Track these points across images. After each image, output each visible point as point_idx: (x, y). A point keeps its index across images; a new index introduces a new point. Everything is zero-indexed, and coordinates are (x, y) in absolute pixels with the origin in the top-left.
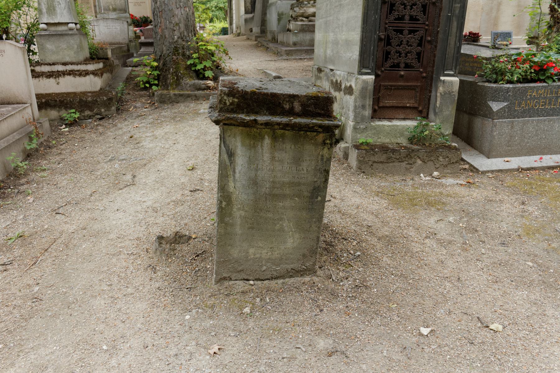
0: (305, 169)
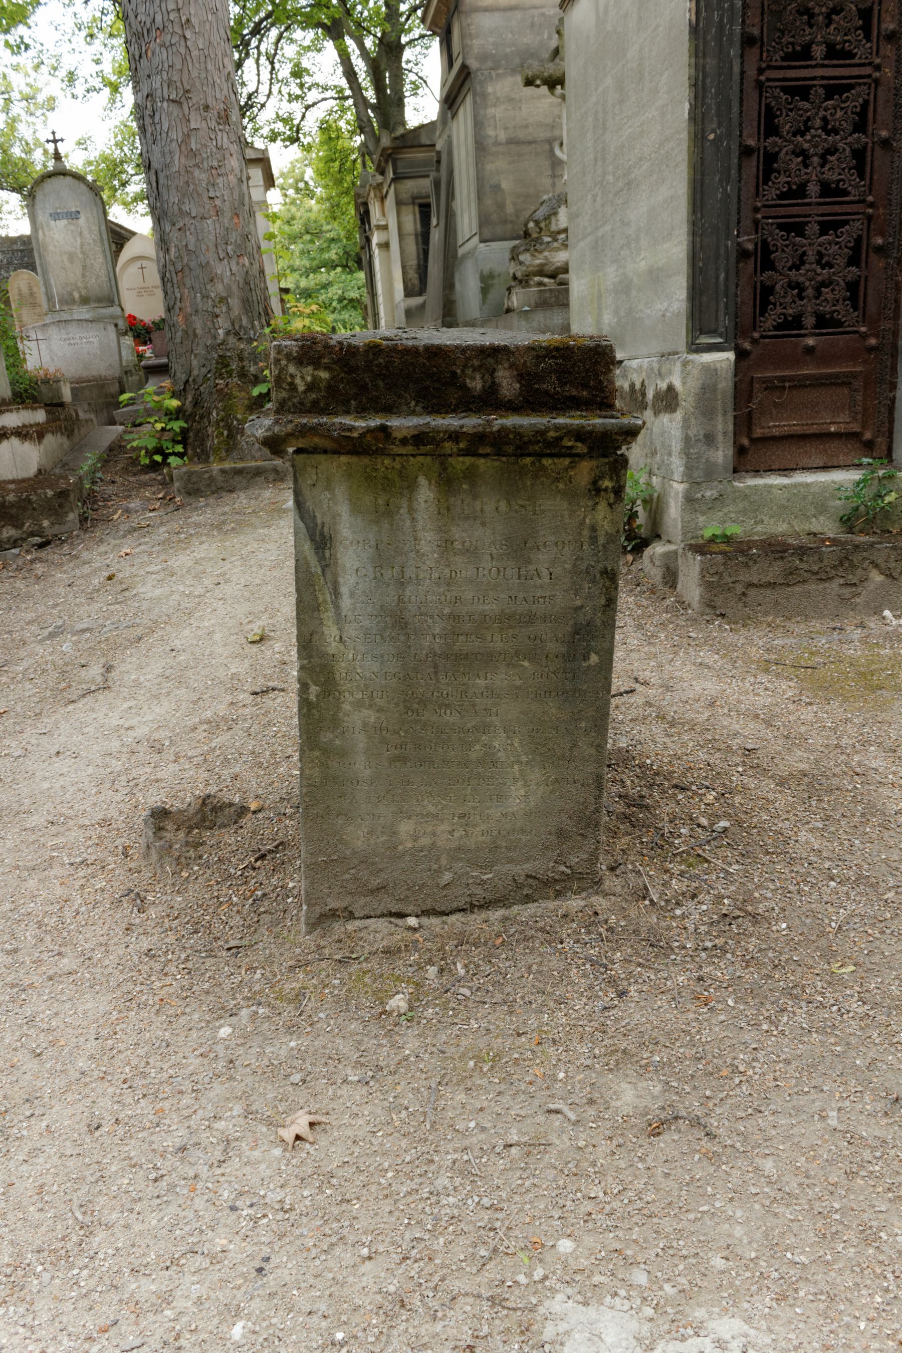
0: (545, 573)
